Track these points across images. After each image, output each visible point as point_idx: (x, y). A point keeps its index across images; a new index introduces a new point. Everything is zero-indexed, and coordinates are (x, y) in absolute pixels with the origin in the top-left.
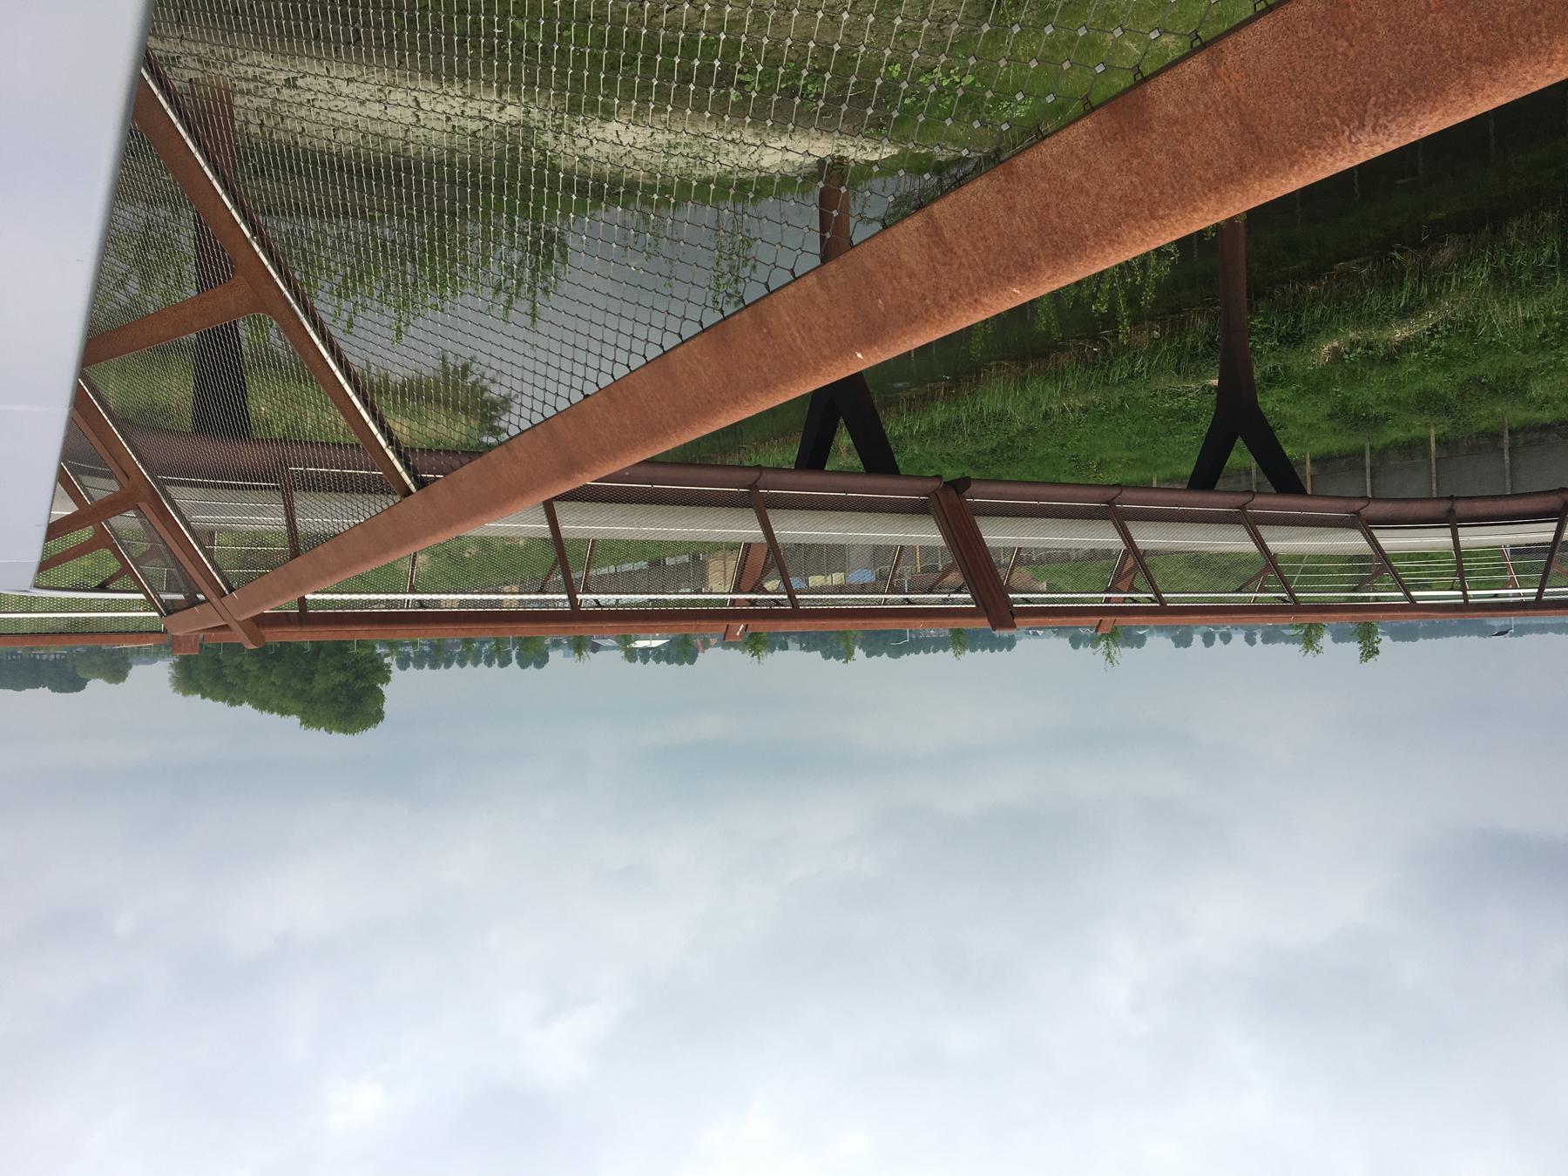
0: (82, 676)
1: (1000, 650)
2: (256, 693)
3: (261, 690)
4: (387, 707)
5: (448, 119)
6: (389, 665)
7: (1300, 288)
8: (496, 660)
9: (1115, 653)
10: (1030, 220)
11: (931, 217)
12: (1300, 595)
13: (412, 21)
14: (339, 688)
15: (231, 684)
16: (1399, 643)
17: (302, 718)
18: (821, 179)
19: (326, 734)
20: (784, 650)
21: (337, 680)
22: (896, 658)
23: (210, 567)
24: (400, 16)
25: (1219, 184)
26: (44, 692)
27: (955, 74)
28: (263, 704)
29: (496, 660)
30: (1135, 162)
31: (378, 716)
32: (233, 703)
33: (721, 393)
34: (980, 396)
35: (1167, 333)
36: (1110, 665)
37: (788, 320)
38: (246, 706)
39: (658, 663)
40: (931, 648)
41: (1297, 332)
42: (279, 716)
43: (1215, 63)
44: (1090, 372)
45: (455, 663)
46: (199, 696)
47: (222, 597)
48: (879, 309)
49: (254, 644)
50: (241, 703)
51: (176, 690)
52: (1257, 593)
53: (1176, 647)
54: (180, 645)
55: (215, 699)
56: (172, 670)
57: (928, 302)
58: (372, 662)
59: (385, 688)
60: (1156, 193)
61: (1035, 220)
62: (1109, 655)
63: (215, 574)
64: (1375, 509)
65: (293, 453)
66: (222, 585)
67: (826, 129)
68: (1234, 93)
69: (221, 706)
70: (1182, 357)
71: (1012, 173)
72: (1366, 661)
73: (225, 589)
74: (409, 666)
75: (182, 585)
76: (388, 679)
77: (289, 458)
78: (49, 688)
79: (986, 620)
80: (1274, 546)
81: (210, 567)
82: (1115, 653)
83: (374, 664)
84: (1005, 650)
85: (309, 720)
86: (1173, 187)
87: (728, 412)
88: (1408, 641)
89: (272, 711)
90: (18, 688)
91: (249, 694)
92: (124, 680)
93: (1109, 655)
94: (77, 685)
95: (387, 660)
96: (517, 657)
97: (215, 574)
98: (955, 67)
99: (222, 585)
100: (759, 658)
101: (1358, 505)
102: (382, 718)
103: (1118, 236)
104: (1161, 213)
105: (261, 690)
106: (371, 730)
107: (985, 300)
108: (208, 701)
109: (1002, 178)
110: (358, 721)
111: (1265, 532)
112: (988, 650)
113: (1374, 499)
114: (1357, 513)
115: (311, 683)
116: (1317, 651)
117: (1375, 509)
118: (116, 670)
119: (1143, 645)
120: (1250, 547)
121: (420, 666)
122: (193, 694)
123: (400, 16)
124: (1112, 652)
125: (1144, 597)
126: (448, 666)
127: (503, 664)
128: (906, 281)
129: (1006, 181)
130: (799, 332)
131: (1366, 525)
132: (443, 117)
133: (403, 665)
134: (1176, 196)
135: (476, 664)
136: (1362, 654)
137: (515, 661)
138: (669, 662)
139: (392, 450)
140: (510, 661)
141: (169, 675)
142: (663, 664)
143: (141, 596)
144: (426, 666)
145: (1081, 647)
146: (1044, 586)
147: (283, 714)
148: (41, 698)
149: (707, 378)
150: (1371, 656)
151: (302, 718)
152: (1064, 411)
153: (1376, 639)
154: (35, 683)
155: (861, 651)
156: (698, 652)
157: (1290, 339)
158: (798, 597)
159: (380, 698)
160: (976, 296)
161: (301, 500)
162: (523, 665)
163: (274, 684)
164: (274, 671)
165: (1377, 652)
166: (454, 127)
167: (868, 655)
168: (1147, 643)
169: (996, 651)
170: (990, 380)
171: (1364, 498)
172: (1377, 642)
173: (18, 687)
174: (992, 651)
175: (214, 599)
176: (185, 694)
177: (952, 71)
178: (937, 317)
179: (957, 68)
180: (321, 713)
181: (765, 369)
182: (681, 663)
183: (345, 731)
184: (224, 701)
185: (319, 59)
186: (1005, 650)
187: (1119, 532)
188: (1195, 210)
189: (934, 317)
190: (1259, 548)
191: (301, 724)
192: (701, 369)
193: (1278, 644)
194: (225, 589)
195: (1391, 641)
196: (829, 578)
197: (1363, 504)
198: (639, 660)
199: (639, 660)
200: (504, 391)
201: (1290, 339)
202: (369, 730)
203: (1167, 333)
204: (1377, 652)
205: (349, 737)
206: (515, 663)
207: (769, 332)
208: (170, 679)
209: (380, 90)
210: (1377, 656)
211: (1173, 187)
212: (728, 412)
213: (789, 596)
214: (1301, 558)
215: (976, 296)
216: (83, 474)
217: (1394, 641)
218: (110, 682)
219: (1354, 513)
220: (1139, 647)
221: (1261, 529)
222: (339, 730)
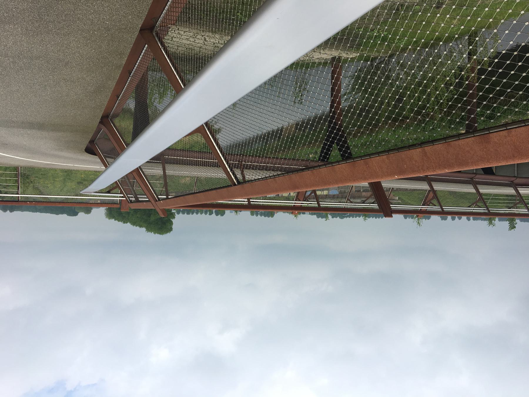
0: (77, 211)
1: (379, 218)
2: (132, 220)
3: (133, 219)
4: (174, 227)
5: (214, 44)
6: (174, 213)
7: (495, 100)
8: (208, 212)
9: (421, 222)
10: (453, 156)
11: (424, 150)
12: (490, 209)
13: (207, 14)
14: (159, 220)
15: (124, 216)
16: (69, 217)
17: (146, 229)
18: (354, 91)
19: (154, 234)
20: (304, 214)
21: (158, 217)
22: (342, 219)
23: (153, 192)
24: (204, 13)
25: (506, 158)
26: (65, 216)
27: (381, 32)
28: (134, 224)
29: (208, 212)
30: (485, 150)
31: (171, 230)
32: (124, 223)
33: (350, 178)
34: (379, 133)
35: (446, 114)
36: (419, 226)
37: (375, 165)
38: (129, 224)
39: (261, 216)
40: (355, 216)
41: (493, 116)
42: (139, 228)
43: (509, 134)
44: (418, 127)
45: (195, 213)
46: (114, 219)
47: (156, 201)
48: (405, 167)
49: (164, 216)
50: (127, 223)
51: (107, 217)
52: (474, 208)
53: (442, 220)
54: (123, 208)
55: (119, 221)
56: (105, 211)
57: (420, 168)
58: (169, 212)
59: (173, 220)
60: (490, 157)
61: (455, 156)
62: (418, 223)
63: (154, 195)
64: (518, 181)
65: (167, 152)
66: (156, 198)
67: (337, 49)
68: (513, 141)
69: (120, 224)
70: (451, 123)
71: (450, 145)
72: (511, 230)
73: (157, 199)
74: (180, 213)
75: (133, 193)
76: (174, 218)
77: (166, 154)
78: (67, 214)
79: (383, 214)
80: (481, 191)
81: (153, 192)
82: (421, 222)
83: (170, 212)
84: (380, 218)
85: (149, 229)
86: (494, 157)
87: (351, 183)
88: (526, 222)
89: (136, 226)
90: (57, 214)
91: (130, 220)
92: (90, 213)
93: (418, 223)
94: (75, 214)
95: (173, 211)
96: (215, 212)
97: (154, 195)
98: (381, 29)
99: (156, 198)
100: (296, 217)
101: (512, 179)
102: (172, 230)
103: (478, 164)
104: (491, 161)
105: (133, 219)
106: (168, 234)
107: (437, 171)
108: (117, 221)
109: (447, 145)
110: (164, 231)
111: (479, 187)
112: (375, 218)
113: (517, 177)
114: (512, 181)
115: (150, 217)
116: (494, 225)
117: (518, 181)
118: (88, 211)
119: (430, 219)
120: (474, 191)
121: (183, 213)
122: (112, 219)
123: (204, 13)
124: (420, 222)
125: (437, 208)
126: (192, 214)
127: (210, 214)
128: (414, 162)
129: (448, 146)
130: (378, 168)
131: (515, 186)
132: (213, 43)
133: (178, 213)
134: (495, 159)
135: (201, 214)
136: (510, 228)
137: (214, 213)
138: (265, 217)
139: (232, 173)
140: (213, 213)
141: (105, 213)
142: (263, 217)
143: (125, 199)
144: (186, 213)
145: (408, 218)
146: (397, 198)
147: (140, 227)
148: (64, 218)
149: (346, 174)
150: (513, 229)
151: (146, 229)
152: (408, 139)
153: (515, 223)
154: (62, 213)
155: (330, 216)
156: (275, 213)
157: (490, 118)
158: (320, 203)
159: (172, 223)
160: (434, 169)
161: (167, 166)
162: (217, 215)
163: (138, 217)
164: (138, 213)
165: (515, 227)
166: (215, 46)
167: (332, 218)
168: (431, 218)
169: (377, 218)
170: (383, 128)
171: (515, 177)
172: (516, 224)
173: (57, 214)
174: (376, 218)
175: (153, 202)
176: (109, 219)
177: (380, 31)
178: (422, 172)
179: (382, 30)
180: (153, 228)
181: (365, 175)
182: (269, 217)
183: (160, 234)
184: (122, 222)
185: (176, 26)
186: (380, 218)
187: (428, 184)
188: (500, 162)
189: (421, 172)
190: (476, 191)
191: (146, 231)
192: (345, 171)
193: (478, 221)
194: (157, 199)
195: (520, 222)
196: (323, 192)
197: (514, 179)
198: (255, 215)
199: (255, 215)
200: (218, 127)
201: (490, 118)
202: (168, 234)
203: (446, 114)
204: (515, 227)
205: (161, 236)
206: (214, 214)
207: (369, 166)
208: (105, 214)
209: (194, 35)
210: (515, 229)
211: (494, 157)
212: (351, 183)
213: (318, 205)
214: (491, 194)
215: (434, 169)
216: (107, 157)
217: (521, 222)
218: (86, 214)
219: (511, 182)
220: (428, 219)
221: (477, 185)
222: (158, 233)
